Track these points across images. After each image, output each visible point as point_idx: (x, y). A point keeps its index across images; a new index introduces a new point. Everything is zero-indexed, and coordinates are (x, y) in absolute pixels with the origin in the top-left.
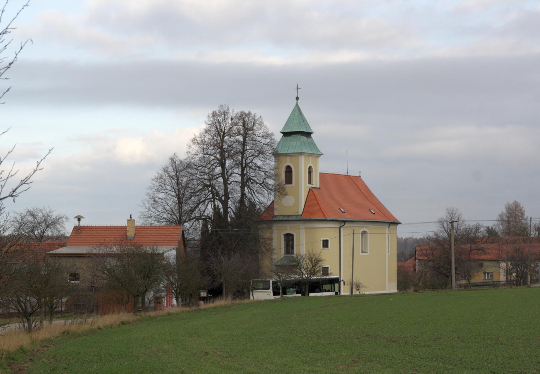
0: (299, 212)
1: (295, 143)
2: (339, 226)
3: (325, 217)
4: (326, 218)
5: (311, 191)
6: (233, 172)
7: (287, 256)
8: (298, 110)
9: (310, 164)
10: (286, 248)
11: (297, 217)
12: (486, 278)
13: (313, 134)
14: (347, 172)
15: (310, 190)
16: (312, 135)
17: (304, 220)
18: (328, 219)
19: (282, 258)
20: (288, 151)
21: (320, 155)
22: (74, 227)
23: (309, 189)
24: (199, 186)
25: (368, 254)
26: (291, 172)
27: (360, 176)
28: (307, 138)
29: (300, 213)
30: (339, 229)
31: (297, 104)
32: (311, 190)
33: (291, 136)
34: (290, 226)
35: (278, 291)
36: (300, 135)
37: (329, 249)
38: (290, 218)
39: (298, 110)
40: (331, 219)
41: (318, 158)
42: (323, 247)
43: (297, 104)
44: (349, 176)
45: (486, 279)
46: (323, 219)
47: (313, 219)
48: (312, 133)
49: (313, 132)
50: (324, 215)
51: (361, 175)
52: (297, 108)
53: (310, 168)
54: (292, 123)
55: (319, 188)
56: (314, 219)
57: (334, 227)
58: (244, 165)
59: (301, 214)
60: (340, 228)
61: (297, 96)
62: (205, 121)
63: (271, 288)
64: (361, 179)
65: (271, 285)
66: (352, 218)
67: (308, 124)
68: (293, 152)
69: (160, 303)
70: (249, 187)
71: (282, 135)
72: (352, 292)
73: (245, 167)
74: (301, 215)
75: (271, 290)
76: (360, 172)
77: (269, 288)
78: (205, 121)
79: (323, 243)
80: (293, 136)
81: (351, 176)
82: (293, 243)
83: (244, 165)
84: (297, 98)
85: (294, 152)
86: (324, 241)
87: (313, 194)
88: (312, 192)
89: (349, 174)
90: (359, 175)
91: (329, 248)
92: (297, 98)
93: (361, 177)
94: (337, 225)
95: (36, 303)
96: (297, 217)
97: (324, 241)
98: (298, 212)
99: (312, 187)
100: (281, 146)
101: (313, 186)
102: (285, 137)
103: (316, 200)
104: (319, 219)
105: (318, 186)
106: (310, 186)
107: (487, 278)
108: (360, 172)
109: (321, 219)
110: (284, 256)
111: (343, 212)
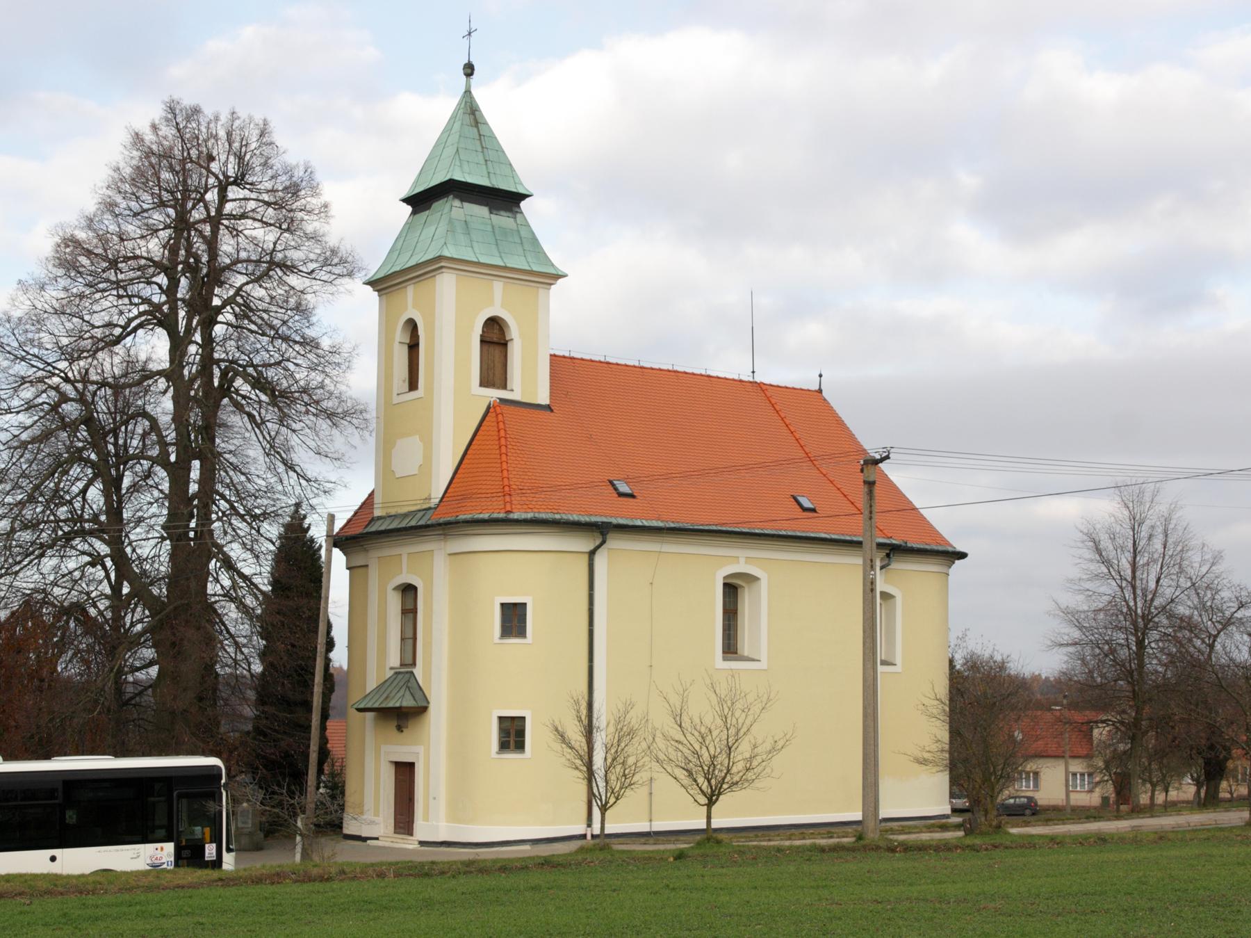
12: (1029, 787)
13: (527, 200)
14: (753, 372)
15: (491, 410)
16: (523, 204)
17: (440, 525)
19: (387, 677)
21: (558, 277)
23: (489, 408)
25: (765, 667)
27: (820, 391)
28: (491, 213)
30: (585, 558)
31: (468, 92)
33: (428, 208)
35: (954, 801)
37: (763, 665)
39: (470, 111)
40: (529, 516)
41: (542, 292)
43: (468, 92)
44: (760, 386)
45: (1031, 788)
47: (462, 517)
48: (524, 197)
49: (522, 191)
51: (822, 388)
55: (548, 408)
60: (592, 553)
64: (825, 400)
66: (658, 519)
67: (511, 165)
71: (409, 209)
72: (709, 822)
76: (821, 376)
80: (436, 205)
81: (764, 384)
84: (469, 70)
89: (758, 379)
90: (817, 388)
91: (725, 659)
92: (469, 70)
93: (825, 394)
94: (582, 544)
95: (1115, 807)
99: (501, 400)
100: (398, 252)
101: (516, 395)
105: (543, 398)
106: (494, 394)
107: (1034, 787)
108: (821, 376)
111: (621, 495)
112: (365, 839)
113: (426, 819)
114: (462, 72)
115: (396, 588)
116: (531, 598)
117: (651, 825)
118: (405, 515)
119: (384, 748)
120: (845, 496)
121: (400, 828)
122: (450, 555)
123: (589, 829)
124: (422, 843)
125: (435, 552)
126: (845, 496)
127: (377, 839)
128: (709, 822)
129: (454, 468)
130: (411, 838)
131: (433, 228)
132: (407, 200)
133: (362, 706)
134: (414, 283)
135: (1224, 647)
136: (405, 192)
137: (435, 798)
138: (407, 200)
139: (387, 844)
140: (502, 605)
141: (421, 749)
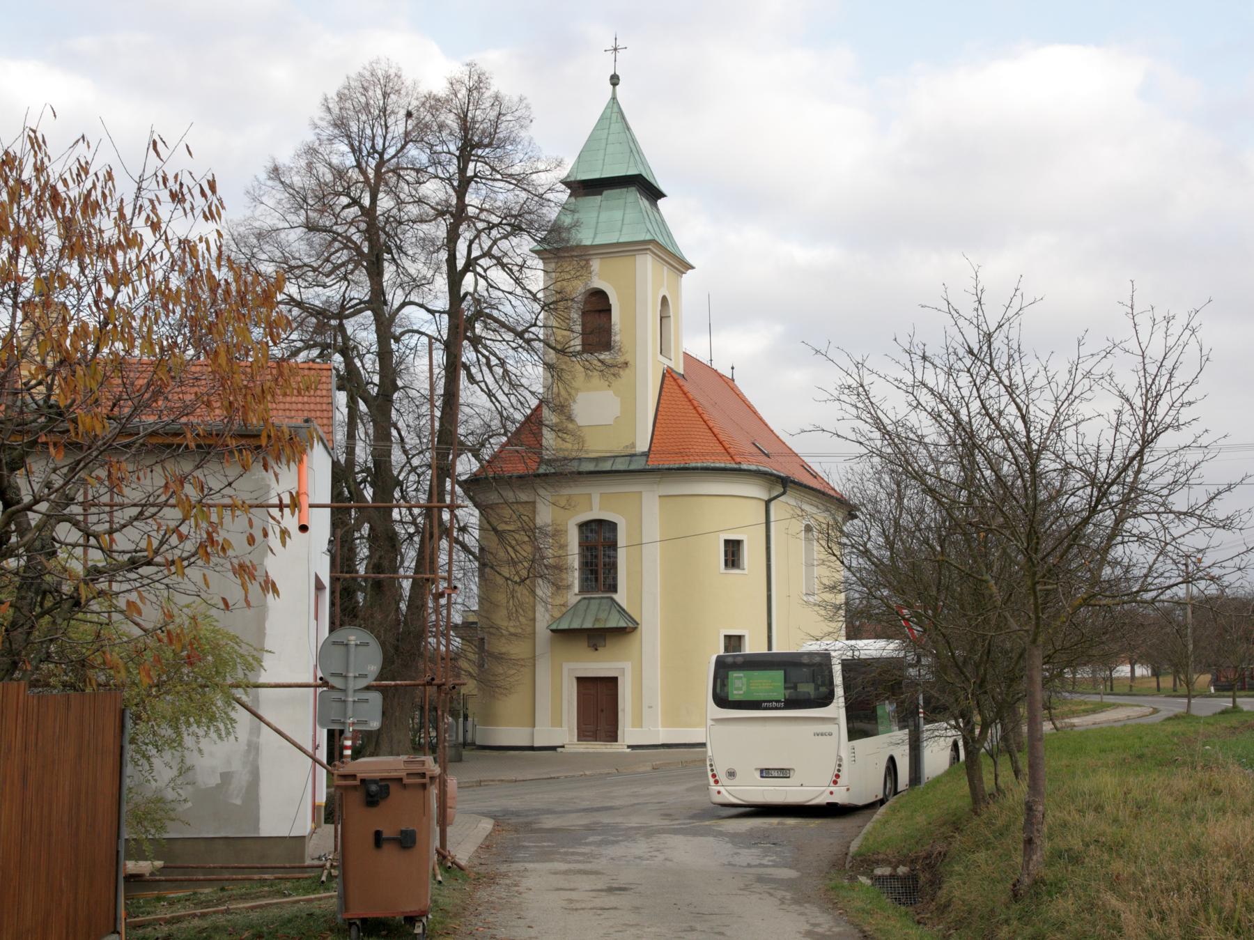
0: (638, 444)
1: (618, 215)
2: (766, 498)
5: (668, 381)
6: (407, 300)
8: (614, 115)
9: (664, 291)
11: (630, 461)
17: (659, 470)
18: (744, 466)
20: (594, 238)
23: (664, 375)
24: (166, 510)
26: (607, 310)
27: (733, 380)
29: (642, 446)
31: (614, 98)
32: (668, 375)
36: (634, 188)
37: (746, 572)
38: (607, 466)
39: (614, 115)
40: (753, 467)
43: (614, 98)
46: (729, 466)
47: (693, 465)
50: (728, 453)
54: (602, 152)
56: (699, 465)
58: (460, 264)
59: (646, 449)
60: (768, 503)
62: (312, 119)
63: (839, 691)
65: (838, 679)
68: (615, 241)
69: (406, 841)
70: (476, 342)
72: (1189, 702)
73: (466, 269)
74: (646, 455)
75: (837, 709)
76: (733, 368)
77: (825, 700)
78: (312, 119)
83: (460, 264)
84: (615, 80)
85: (621, 240)
87: (676, 387)
88: (673, 383)
92: (615, 80)
93: (736, 382)
94: (756, 491)
96: (630, 461)
98: (633, 445)
102: (579, 199)
103: (691, 407)
104: (718, 465)
108: (733, 368)
109: (723, 465)
110: (579, 598)
112: (554, 748)
117: (533, 734)
118: (597, 460)
119: (567, 667)
121: (585, 736)
124: (629, 747)
125: (644, 495)
127: (563, 747)
128: (1189, 702)
133: (564, 626)
137: (650, 707)
139: (572, 750)
141: (627, 666)
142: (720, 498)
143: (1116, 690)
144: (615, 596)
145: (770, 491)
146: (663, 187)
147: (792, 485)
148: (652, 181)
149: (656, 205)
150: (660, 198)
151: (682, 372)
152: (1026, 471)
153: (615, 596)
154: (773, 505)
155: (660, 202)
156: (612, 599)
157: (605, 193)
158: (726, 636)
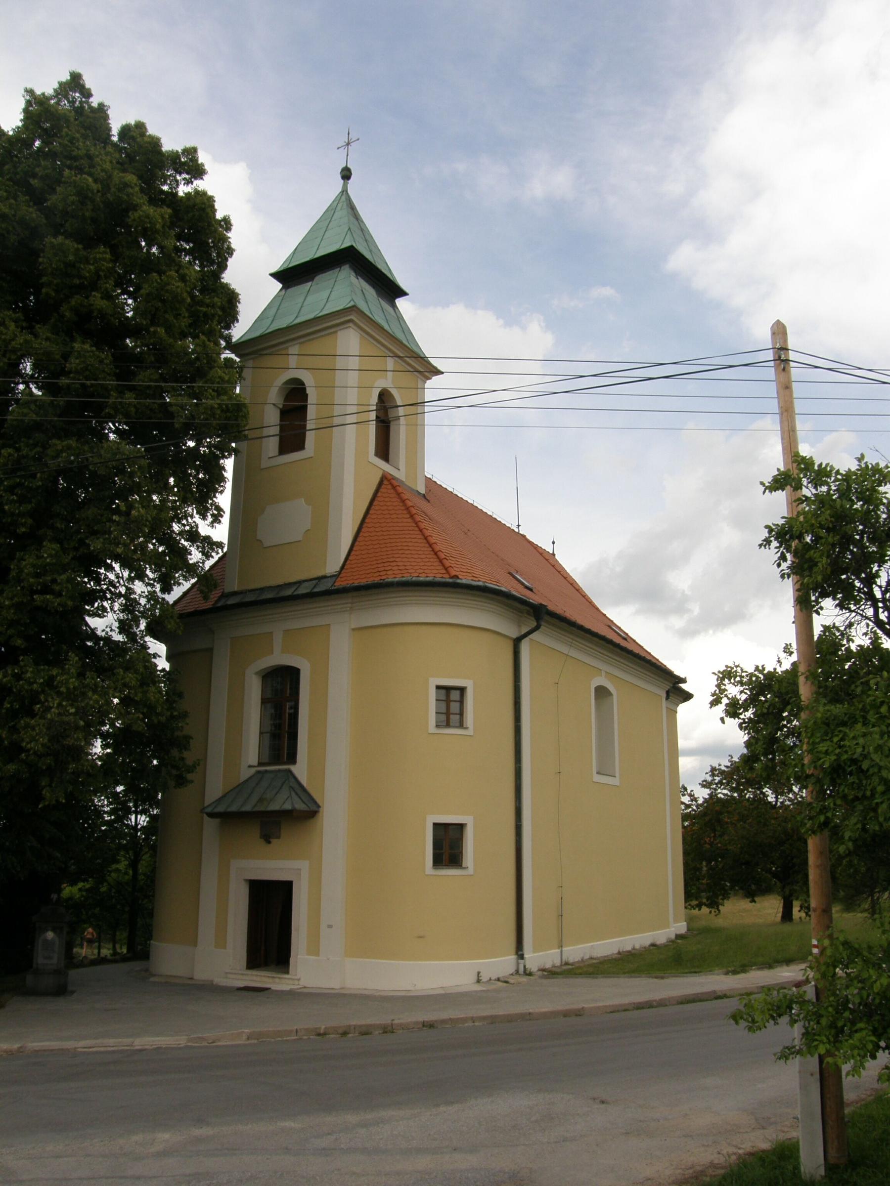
2: (515, 635)
3: (448, 572)
4: (457, 577)
7: (266, 771)
8: (345, 203)
9: (386, 382)
10: (267, 737)
15: (385, 482)
22: (298, 761)
23: (381, 484)
27: (553, 554)
29: (333, 566)
31: (344, 191)
34: (286, 631)
37: (470, 732)
38: (289, 592)
39: (345, 203)
42: (438, 861)
43: (344, 191)
52: (343, 198)
53: (384, 397)
57: (503, 632)
61: (344, 165)
74: (336, 576)
76: (553, 543)
79: (437, 845)
82: (296, 708)
84: (346, 174)
86: (440, 829)
92: (346, 174)
97: (440, 829)
102: (289, 290)
108: (553, 543)
110: (253, 770)
113: (314, 949)
114: (339, 176)
115: (257, 673)
116: (471, 818)
120: (547, 560)
122: (353, 630)
123: (521, 961)
126: (547, 560)
129: (354, 534)
130: (286, 976)
131: (325, 294)
132: (277, 276)
134: (300, 343)
135: (861, 1029)
136: (276, 267)
137: (330, 926)
138: (277, 276)
140: (435, 825)
142: (424, 627)
143: (451, 724)
144: (293, 768)
145: (519, 626)
146: (402, 281)
147: (546, 617)
148: (380, 266)
149: (394, 306)
150: (399, 297)
151: (423, 491)
152: (881, 608)
153: (293, 768)
154: (525, 646)
155: (400, 302)
156: (290, 771)
157: (317, 278)
158: (435, 825)
